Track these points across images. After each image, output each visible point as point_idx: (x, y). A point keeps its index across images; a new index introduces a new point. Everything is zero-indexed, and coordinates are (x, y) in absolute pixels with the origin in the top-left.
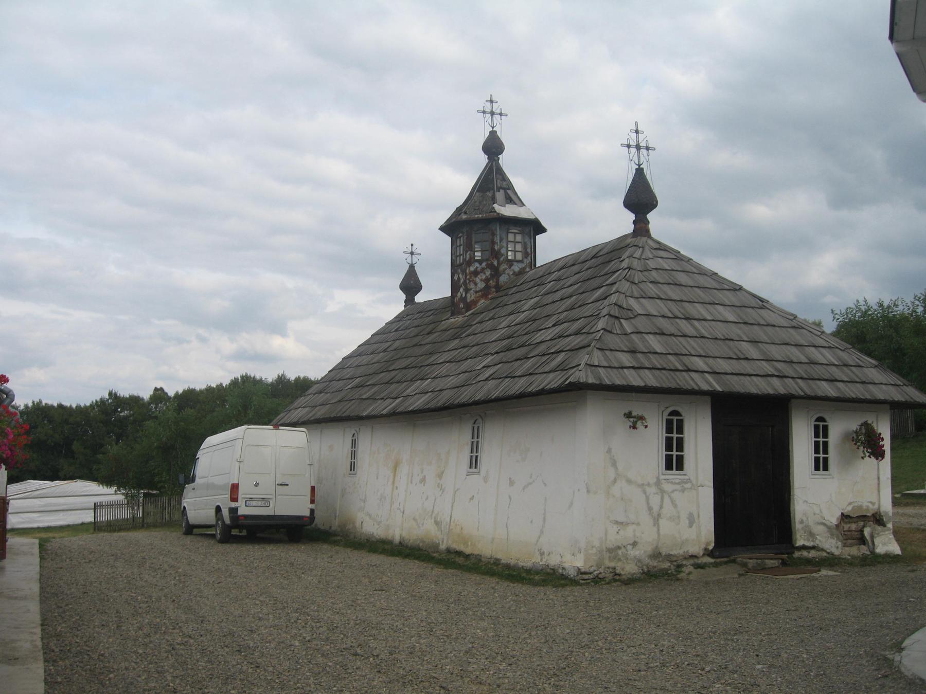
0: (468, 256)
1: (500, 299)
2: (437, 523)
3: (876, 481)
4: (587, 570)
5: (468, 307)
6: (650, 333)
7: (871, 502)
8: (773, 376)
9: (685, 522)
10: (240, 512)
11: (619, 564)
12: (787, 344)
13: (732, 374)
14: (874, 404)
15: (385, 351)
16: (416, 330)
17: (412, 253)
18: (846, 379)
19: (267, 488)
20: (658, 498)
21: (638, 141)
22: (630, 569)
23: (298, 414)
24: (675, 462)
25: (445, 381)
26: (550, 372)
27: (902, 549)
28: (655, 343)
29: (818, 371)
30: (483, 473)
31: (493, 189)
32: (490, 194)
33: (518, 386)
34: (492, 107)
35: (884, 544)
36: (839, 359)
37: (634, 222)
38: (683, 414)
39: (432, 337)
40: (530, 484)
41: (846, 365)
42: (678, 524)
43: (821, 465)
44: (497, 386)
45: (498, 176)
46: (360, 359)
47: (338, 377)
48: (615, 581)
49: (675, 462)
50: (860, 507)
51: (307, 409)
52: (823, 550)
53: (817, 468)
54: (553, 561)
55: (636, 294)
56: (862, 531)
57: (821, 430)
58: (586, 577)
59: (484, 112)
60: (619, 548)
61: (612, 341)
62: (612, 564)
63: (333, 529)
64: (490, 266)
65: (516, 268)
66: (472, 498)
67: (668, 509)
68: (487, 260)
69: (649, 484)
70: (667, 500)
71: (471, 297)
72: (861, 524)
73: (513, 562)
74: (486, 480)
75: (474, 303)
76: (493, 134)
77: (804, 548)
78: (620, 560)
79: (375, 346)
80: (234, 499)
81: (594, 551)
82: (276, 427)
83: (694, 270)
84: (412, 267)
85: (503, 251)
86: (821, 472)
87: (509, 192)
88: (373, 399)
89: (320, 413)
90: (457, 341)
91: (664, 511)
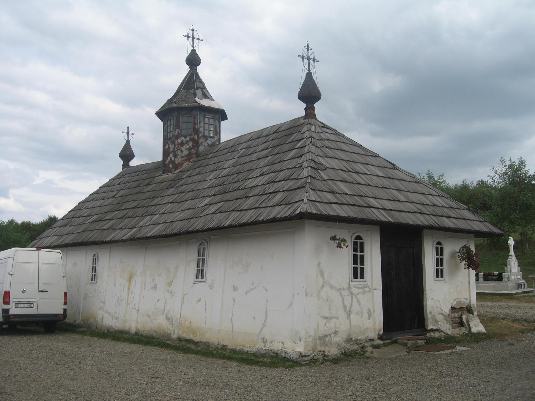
0: (177, 132)
1: (201, 162)
2: (168, 318)
3: (468, 284)
4: (307, 354)
5: (176, 167)
6: (339, 181)
7: (465, 298)
8: (418, 213)
9: (366, 315)
10: (11, 312)
11: (327, 348)
12: (416, 192)
13: (395, 210)
15: (113, 197)
16: (136, 184)
17: (128, 133)
18: (455, 217)
19: (32, 294)
21: (308, 54)
22: (333, 351)
24: (359, 273)
25: (173, 214)
26: (275, 206)
27: (485, 327)
28: (343, 187)
29: (439, 211)
30: (209, 281)
31: (194, 88)
32: (192, 91)
33: (231, 219)
34: (193, 34)
35: (476, 326)
36: (447, 203)
37: (306, 109)
38: (363, 238)
39: (150, 188)
40: (253, 289)
41: (451, 208)
42: (362, 317)
43: (440, 274)
44: (226, 218)
45: (197, 80)
46: (92, 204)
47: (78, 215)
48: (326, 361)
49: (359, 273)
50: (460, 302)
51: (56, 237)
52: (442, 331)
53: (355, 276)
54: (276, 347)
55: (321, 155)
56: (461, 318)
57: (439, 251)
58: (306, 359)
59: (188, 37)
60: (326, 336)
61: (319, 185)
62: (322, 349)
63: (77, 322)
64: (193, 140)
65: (210, 141)
66: (199, 300)
67: (356, 307)
68: (190, 135)
69: (344, 289)
70: (355, 299)
71: (178, 160)
72: (460, 313)
73: (238, 348)
74: (211, 287)
75: (181, 164)
76: (193, 51)
77: (432, 330)
78: (327, 345)
79: (104, 194)
80: (6, 302)
81: (311, 339)
82: (39, 249)
83: (349, 143)
85: (201, 129)
86: (440, 279)
88: (112, 229)
89: (68, 239)
90: (173, 189)
91: (353, 308)
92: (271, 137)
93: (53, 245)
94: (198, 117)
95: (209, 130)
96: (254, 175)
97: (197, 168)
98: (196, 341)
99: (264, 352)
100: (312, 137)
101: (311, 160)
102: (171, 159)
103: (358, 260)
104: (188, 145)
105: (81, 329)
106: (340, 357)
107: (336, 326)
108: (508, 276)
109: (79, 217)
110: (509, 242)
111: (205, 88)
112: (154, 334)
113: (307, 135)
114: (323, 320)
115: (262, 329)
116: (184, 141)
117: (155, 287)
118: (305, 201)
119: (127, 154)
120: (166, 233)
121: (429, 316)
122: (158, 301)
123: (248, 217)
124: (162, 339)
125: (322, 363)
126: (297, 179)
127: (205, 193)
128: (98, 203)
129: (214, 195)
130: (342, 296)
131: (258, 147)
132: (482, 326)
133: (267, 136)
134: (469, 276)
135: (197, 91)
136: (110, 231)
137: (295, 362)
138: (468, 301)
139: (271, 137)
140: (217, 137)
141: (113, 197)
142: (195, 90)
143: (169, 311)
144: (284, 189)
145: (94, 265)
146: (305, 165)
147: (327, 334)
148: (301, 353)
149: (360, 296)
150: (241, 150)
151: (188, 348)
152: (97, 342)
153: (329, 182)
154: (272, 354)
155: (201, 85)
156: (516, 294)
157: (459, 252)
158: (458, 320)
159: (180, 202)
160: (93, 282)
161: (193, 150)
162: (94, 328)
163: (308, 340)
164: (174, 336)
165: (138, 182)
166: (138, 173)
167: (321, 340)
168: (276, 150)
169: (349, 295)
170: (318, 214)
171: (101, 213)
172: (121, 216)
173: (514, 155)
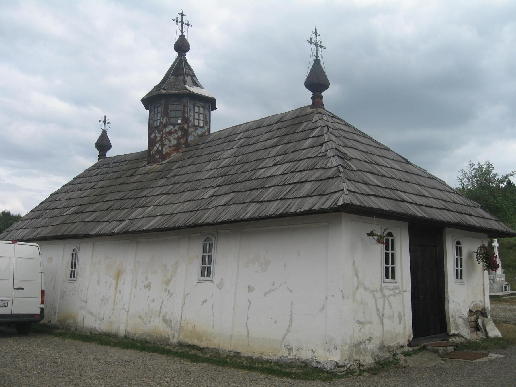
0: (165, 121)
2: (165, 321)
3: (482, 286)
5: (163, 157)
9: (397, 320)
11: (362, 357)
12: (435, 188)
13: (425, 206)
14: (492, 234)
15: (91, 188)
16: (117, 174)
17: (105, 122)
20: (382, 300)
21: (316, 40)
22: (368, 360)
23: (21, 233)
24: (390, 273)
26: (306, 197)
31: (183, 75)
32: (181, 78)
33: (250, 211)
34: (182, 18)
35: (492, 330)
37: (313, 98)
38: (394, 235)
39: (135, 179)
40: (273, 290)
42: (393, 322)
43: (459, 275)
45: (186, 67)
46: (67, 195)
47: (52, 206)
49: (390, 273)
50: (475, 305)
51: (28, 230)
52: (462, 336)
54: (305, 355)
56: (476, 322)
57: (459, 251)
59: (177, 21)
60: (361, 343)
62: (357, 357)
63: (53, 322)
64: (182, 129)
65: (200, 131)
66: (205, 301)
67: (388, 312)
69: (376, 291)
71: (166, 150)
72: (475, 316)
73: (255, 356)
74: (220, 286)
75: (169, 155)
76: (182, 37)
77: (454, 335)
78: (362, 353)
81: (347, 347)
82: (15, 241)
84: (104, 132)
85: (191, 118)
86: (459, 280)
87: (194, 78)
89: (45, 232)
91: (385, 312)
92: (275, 127)
93: (26, 238)
94: (189, 105)
95: (199, 120)
96: (266, 164)
97: (189, 158)
98: (202, 347)
99: (289, 361)
100: (327, 126)
101: (336, 149)
102: (158, 149)
103: (390, 259)
104: (177, 134)
105: (59, 331)
106: (374, 366)
107: (370, 332)
108: (494, 278)
109: (53, 209)
110: (493, 244)
111: (194, 76)
112: (148, 338)
113: (320, 123)
114: (358, 325)
115: (286, 335)
116: (173, 130)
117: (148, 286)
118: (346, 192)
119: (103, 144)
120: (167, 226)
121: (451, 320)
122: (153, 301)
123: (272, 209)
124: (158, 343)
125: (360, 374)
126: (324, 168)
127: (207, 183)
128: (75, 195)
129: (219, 186)
130: (375, 298)
131: (260, 137)
132: (498, 330)
133: (269, 125)
134: (483, 277)
135: (186, 78)
136: (95, 223)
137: (329, 372)
138: (483, 304)
139: (275, 127)
140: (206, 128)
141: (91, 188)
142: (184, 77)
143: (166, 313)
144: (312, 179)
145: (74, 261)
146: (330, 153)
147: (361, 341)
148: (337, 363)
149: (391, 298)
150: (240, 139)
151: (195, 355)
152: (87, 347)
153: (359, 172)
154: (299, 363)
155: (191, 72)
156: (503, 296)
157: (477, 252)
158: (474, 324)
159: (176, 193)
160: (72, 279)
161: (182, 140)
162: (73, 329)
163: (345, 348)
164: (174, 341)
165: (120, 173)
166: (117, 164)
167: (356, 348)
168: (286, 139)
169: (381, 298)
170: (357, 206)
171: (80, 205)
172: (106, 208)
173: (481, 159)
